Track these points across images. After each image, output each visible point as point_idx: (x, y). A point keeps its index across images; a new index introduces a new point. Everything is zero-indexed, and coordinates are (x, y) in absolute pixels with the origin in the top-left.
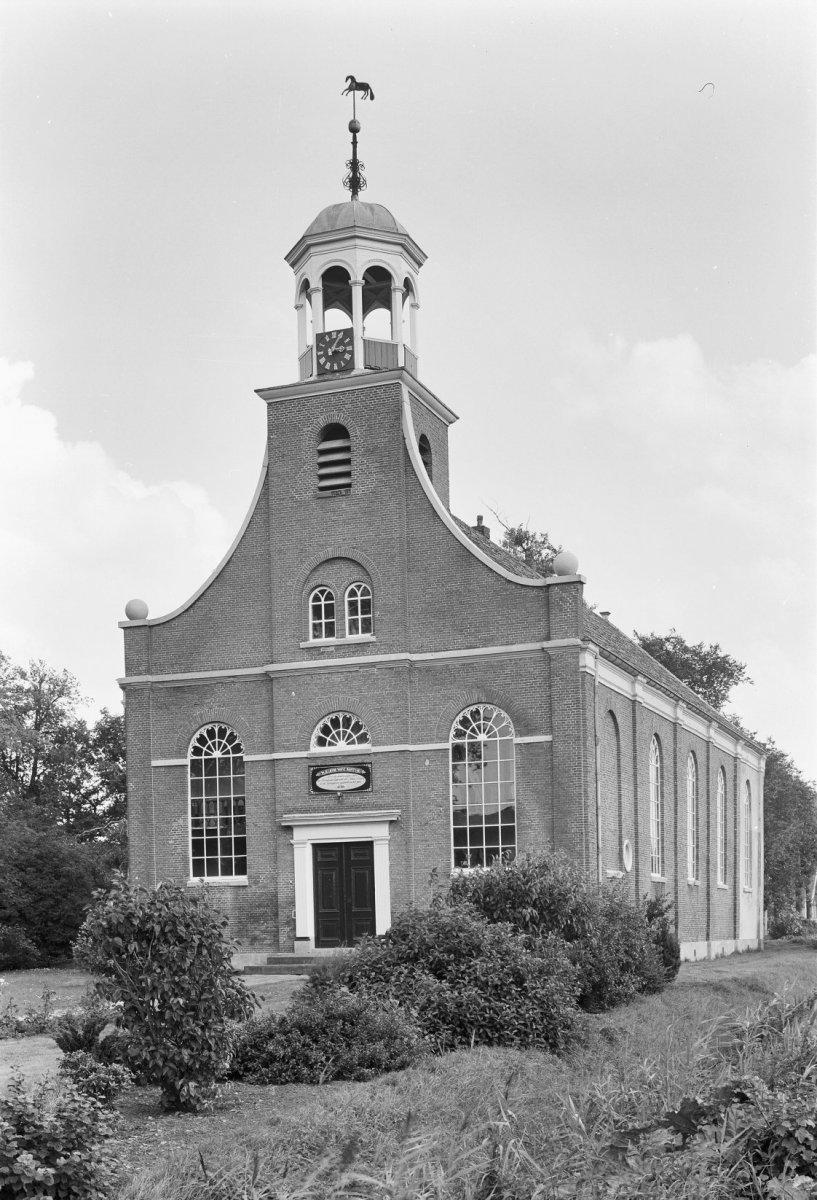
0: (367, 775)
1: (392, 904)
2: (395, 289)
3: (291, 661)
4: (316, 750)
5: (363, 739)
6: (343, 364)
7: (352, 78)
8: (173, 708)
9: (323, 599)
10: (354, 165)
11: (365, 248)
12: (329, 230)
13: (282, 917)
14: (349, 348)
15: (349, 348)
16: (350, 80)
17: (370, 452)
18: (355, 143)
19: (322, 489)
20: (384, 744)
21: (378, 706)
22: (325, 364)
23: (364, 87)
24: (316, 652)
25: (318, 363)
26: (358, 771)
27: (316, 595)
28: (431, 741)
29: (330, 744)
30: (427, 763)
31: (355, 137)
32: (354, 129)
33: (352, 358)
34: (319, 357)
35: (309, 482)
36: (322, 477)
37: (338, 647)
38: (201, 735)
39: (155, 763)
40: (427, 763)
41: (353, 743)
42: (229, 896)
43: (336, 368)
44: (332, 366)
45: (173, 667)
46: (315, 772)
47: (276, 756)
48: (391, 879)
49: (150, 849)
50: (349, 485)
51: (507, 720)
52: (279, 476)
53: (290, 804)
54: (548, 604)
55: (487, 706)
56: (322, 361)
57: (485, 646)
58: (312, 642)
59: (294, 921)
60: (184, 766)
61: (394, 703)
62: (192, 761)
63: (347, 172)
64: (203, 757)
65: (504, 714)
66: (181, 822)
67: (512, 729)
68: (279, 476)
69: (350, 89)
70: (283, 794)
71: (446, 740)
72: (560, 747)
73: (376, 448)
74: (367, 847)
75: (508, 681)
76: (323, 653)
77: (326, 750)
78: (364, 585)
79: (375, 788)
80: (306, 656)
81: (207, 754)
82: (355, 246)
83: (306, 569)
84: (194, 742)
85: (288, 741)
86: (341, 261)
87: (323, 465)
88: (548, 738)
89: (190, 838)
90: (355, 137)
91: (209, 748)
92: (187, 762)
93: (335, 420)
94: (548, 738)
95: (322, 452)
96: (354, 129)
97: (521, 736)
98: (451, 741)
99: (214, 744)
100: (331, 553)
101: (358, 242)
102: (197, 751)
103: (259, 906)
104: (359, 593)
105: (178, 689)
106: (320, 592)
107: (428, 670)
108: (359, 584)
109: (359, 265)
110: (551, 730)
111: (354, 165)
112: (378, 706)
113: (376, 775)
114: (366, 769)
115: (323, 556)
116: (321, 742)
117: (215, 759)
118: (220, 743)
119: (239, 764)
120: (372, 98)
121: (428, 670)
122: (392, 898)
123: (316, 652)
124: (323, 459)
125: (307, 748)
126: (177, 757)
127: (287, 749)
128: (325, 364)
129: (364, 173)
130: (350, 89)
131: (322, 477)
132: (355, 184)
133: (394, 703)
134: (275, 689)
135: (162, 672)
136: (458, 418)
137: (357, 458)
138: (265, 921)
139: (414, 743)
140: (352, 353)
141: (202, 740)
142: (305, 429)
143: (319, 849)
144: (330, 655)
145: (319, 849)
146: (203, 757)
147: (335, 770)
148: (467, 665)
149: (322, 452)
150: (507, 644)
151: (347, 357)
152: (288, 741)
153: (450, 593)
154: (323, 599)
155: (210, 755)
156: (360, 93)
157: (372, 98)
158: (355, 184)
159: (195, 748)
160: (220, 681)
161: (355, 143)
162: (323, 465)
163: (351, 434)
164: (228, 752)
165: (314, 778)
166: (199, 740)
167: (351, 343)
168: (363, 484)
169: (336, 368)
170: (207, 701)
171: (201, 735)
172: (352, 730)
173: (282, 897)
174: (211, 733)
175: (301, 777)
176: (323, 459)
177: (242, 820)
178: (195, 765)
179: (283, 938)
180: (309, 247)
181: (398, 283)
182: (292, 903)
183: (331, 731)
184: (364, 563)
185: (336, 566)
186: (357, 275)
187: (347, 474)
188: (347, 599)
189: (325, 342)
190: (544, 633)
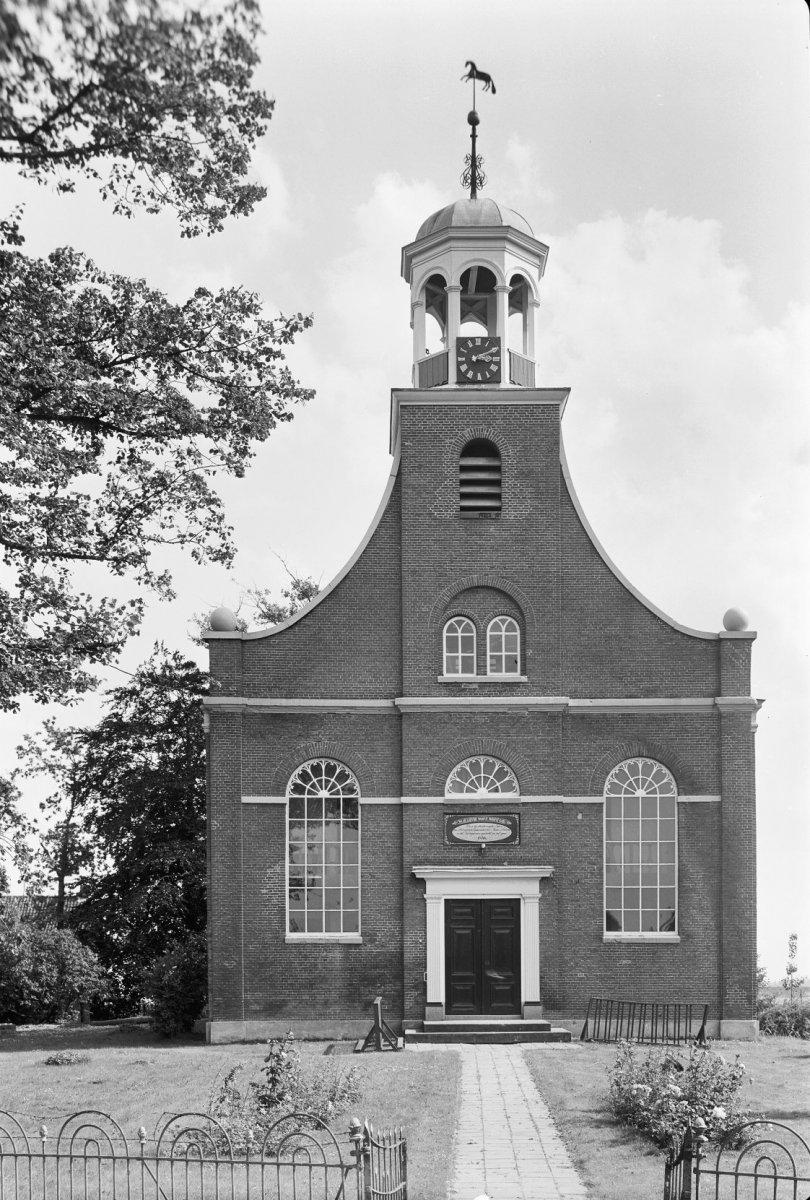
1: (541, 968)
3: (425, 695)
4: (451, 796)
6: (488, 376)
7: (473, 66)
8: (270, 737)
9: (460, 631)
10: (474, 161)
11: (457, 249)
12: (439, 231)
13: (408, 980)
14: (495, 359)
15: (495, 359)
16: (469, 67)
17: (524, 475)
18: (474, 136)
19: (463, 509)
20: (534, 794)
21: (529, 752)
22: (467, 371)
23: (485, 77)
24: (456, 688)
25: (459, 370)
26: (503, 821)
27: (496, 623)
28: (584, 794)
29: (469, 790)
30: (580, 817)
31: (474, 130)
32: (473, 120)
33: (499, 370)
34: (459, 364)
35: (448, 502)
36: (464, 496)
37: (483, 685)
39: (245, 799)
40: (580, 817)
41: (496, 790)
42: (338, 955)
43: (479, 378)
44: (475, 375)
45: (271, 691)
47: (405, 800)
48: (541, 941)
49: (239, 899)
50: (498, 509)
51: (668, 778)
52: (414, 488)
53: (421, 855)
54: (718, 658)
55: (647, 760)
56: (464, 368)
57: (646, 697)
59: (425, 984)
60: (283, 805)
61: (547, 751)
62: (292, 800)
63: (464, 167)
64: (306, 796)
65: (665, 770)
66: (277, 869)
67: (674, 786)
68: (414, 488)
69: (471, 75)
70: (410, 841)
71: (600, 793)
72: (729, 808)
73: (531, 472)
74: (512, 906)
75: (673, 736)
76: (464, 690)
78: (510, 619)
79: (524, 841)
80: (444, 692)
81: (310, 792)
82: (450, 250)
83: (445, 595)
84: (294, 778)
85: (420, 784)
86: (487, 262)
87: (464, 483)
88: (717, 798)
89: (287, 888)
90: (474, 130)
92: (285, 800)
93: (485, 434)
94: (717, 798)
95: (464, 469)
96: (473, 120)
97: (685, 795)
98: (605, 795)
100: (476, 579)
101: (508, 246)
102: (298, 789)
103: (376, 967)
104: (504, 628)
105: (279, 720)
106: (456, 622)
107: (583, 717)
108: (504, 617)
110: (720, 790)
111: (474, 161)
112: (529, 752)
114: (513, 820)
115: (466, 582)
116: (458, 788)
117: (321, 799)
120: (494, 91)
121: (583, 719)
122: (541, 962)
123: (456, 688)
124: (464, 476)
125: (442, 795)
126: (274, 795)
127: (419, 794)
128: (467, 371)
129: (484, 169)
130: (471, 75)
131: (464, 496)
132: (474, 181)
133: (547, 751)
134: (404, 726)
135: (256, 695)
137: (508, 482)
138: (383, 984)
139: (565, 794)
140: (498, 364)
141: (304, 776)
142: (447, 441)
143: (451, 905)
144: (472, 693)
145: (451, 905)
146: (306, 796)
147: (475, 819)
148: (628, 718)
149: (464, 469)
150: (672, 697)
151: (494, 368)
152: (420, 784)
153: (608, 638)
154: (460, 631)
155: (315, 794)
156: (481, 84)
157: (494, 91)
158: (474, 181)
159: (295, 785)
160: (334, 715)
161: (474, 136)
162: (464, 483)
163: (503, 452)
164: (654, 792)
166: (459, 774)
167: (498, 354)
168: (515, 509)
169: (479, 378)
170: (314, 733)
171: (304, 771)
172: (316, 777)
173: (408, 957)
174: (316, 770)
176: (464, 476)
179: (408, 1004)
180: (505, 239)
182: (423, 964)
183: (311, 780)
184: (515, 596)
185: (480, 596)
186: (453, 280)
187: (497, 497)
188: (445, 634)
189: (467, 347)
190: (712, 688)
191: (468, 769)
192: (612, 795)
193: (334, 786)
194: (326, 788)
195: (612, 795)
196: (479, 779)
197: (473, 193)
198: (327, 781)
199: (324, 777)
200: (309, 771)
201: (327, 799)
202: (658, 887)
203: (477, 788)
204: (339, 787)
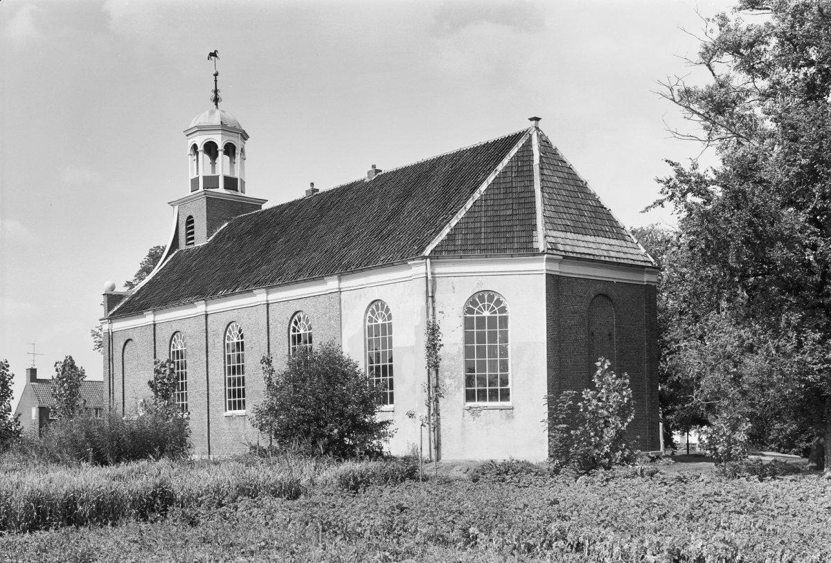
18: (216, 81)
64: (475, 315)
81: (478, 313)
111: (216, 91)
117: (485, 317)
146: (475, 315)
161: (216, 81)
191: (471, 306)
192: (468, 315)
193: (493, 308)
194: (490, 311)
195: (468, 315)
196: (480, 308)
197: (216, 104)
198: (480, 308)
199: (480, 305)
200: (502, 305)
201: (489, 317)
202: (498, 344)
203: (490, 311)
204: (496, 309)
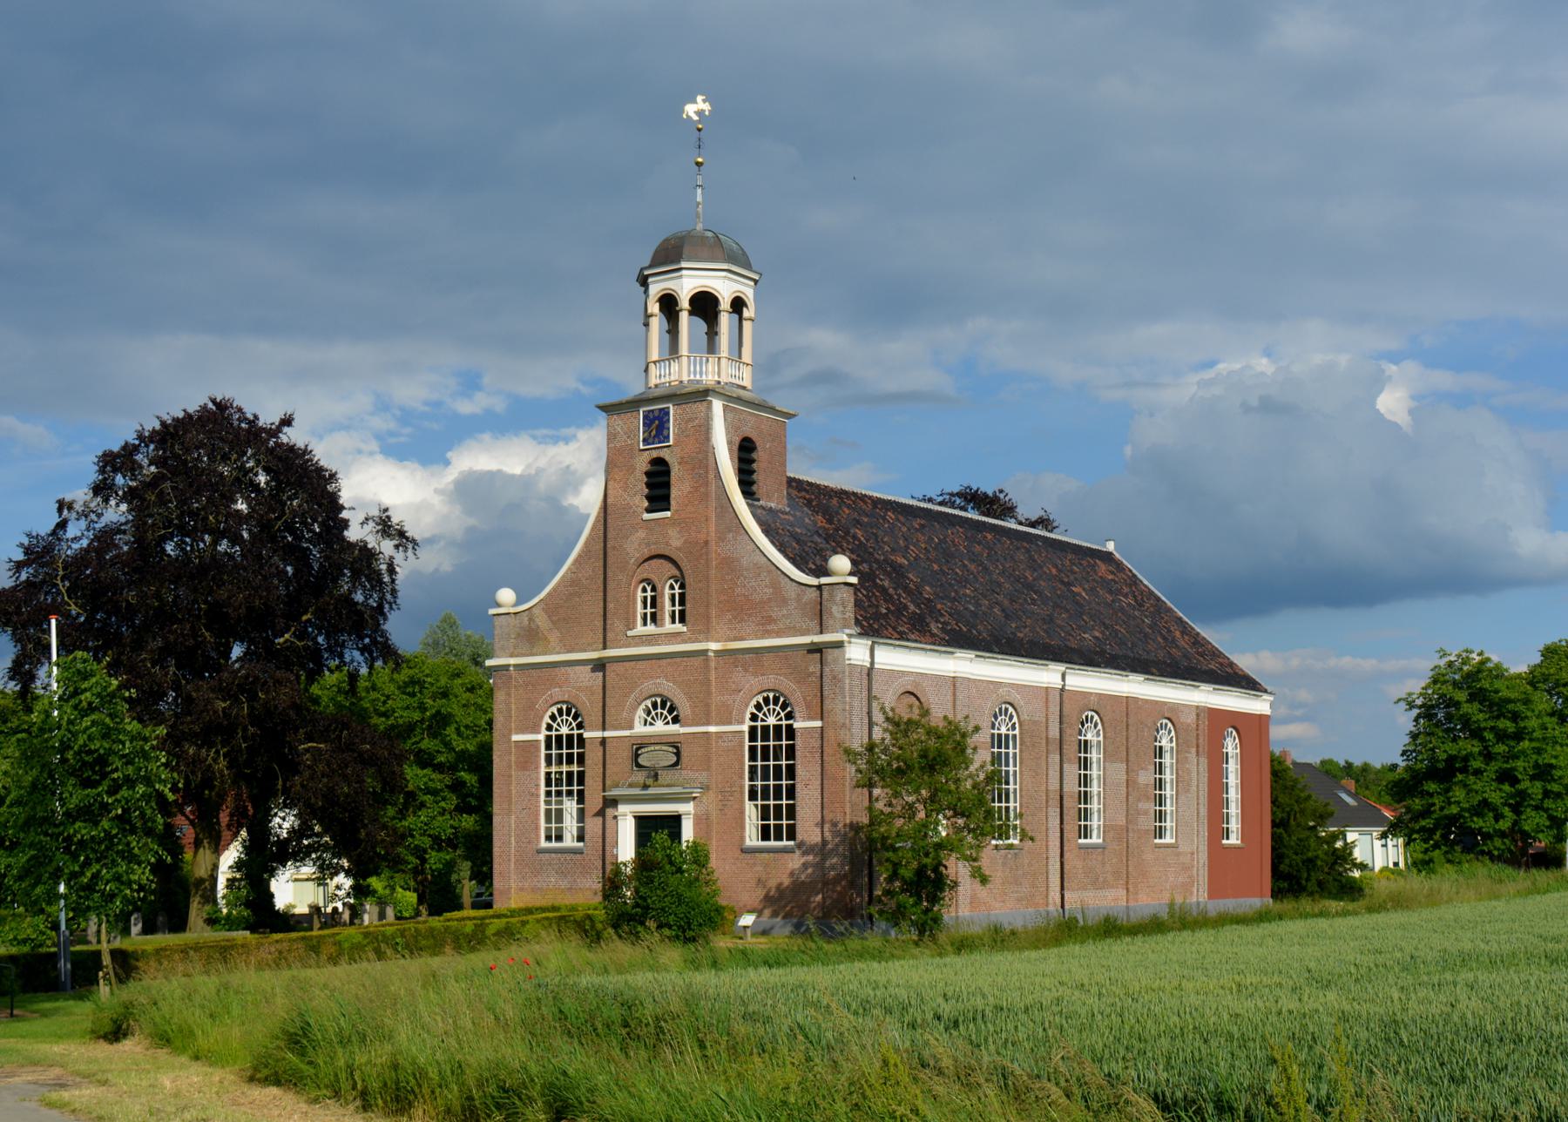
0: (678, 754)
2: (681, 310)
5: (676, 720)
38: (758, 702)
39: (515, 738)
41: (668, 723)
46: (637, 749)
58: (640, 629)
64: (759, 724)
77: (649, 730)
79: (684, 766)
82: (681, 277)
88: (818, 724)
91: (764, 714)
99: (769, 710)
109: (685, 291)
113: (684, 754)
114: (677, 748)
117: (769, 726)
118: (774, 710)
119: (791, 732)
125: (631, 727)
136: (789, 416)
152: (616, 720)
165: (637, 756)
171: (758, 702)
175: (626, 754)
177: (793, 786)
178: (753, 730)
181: (725, 305)
